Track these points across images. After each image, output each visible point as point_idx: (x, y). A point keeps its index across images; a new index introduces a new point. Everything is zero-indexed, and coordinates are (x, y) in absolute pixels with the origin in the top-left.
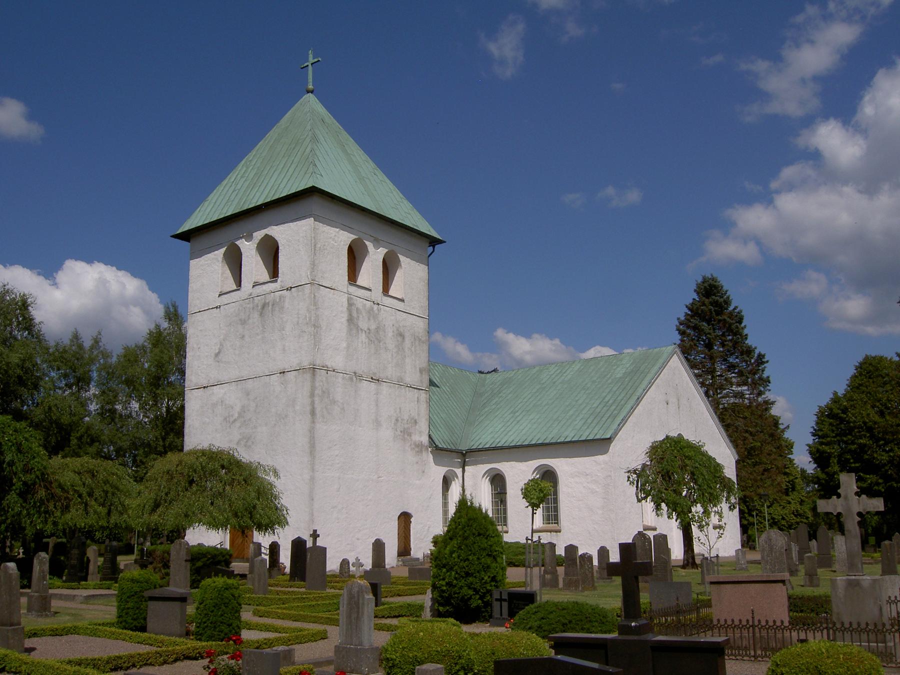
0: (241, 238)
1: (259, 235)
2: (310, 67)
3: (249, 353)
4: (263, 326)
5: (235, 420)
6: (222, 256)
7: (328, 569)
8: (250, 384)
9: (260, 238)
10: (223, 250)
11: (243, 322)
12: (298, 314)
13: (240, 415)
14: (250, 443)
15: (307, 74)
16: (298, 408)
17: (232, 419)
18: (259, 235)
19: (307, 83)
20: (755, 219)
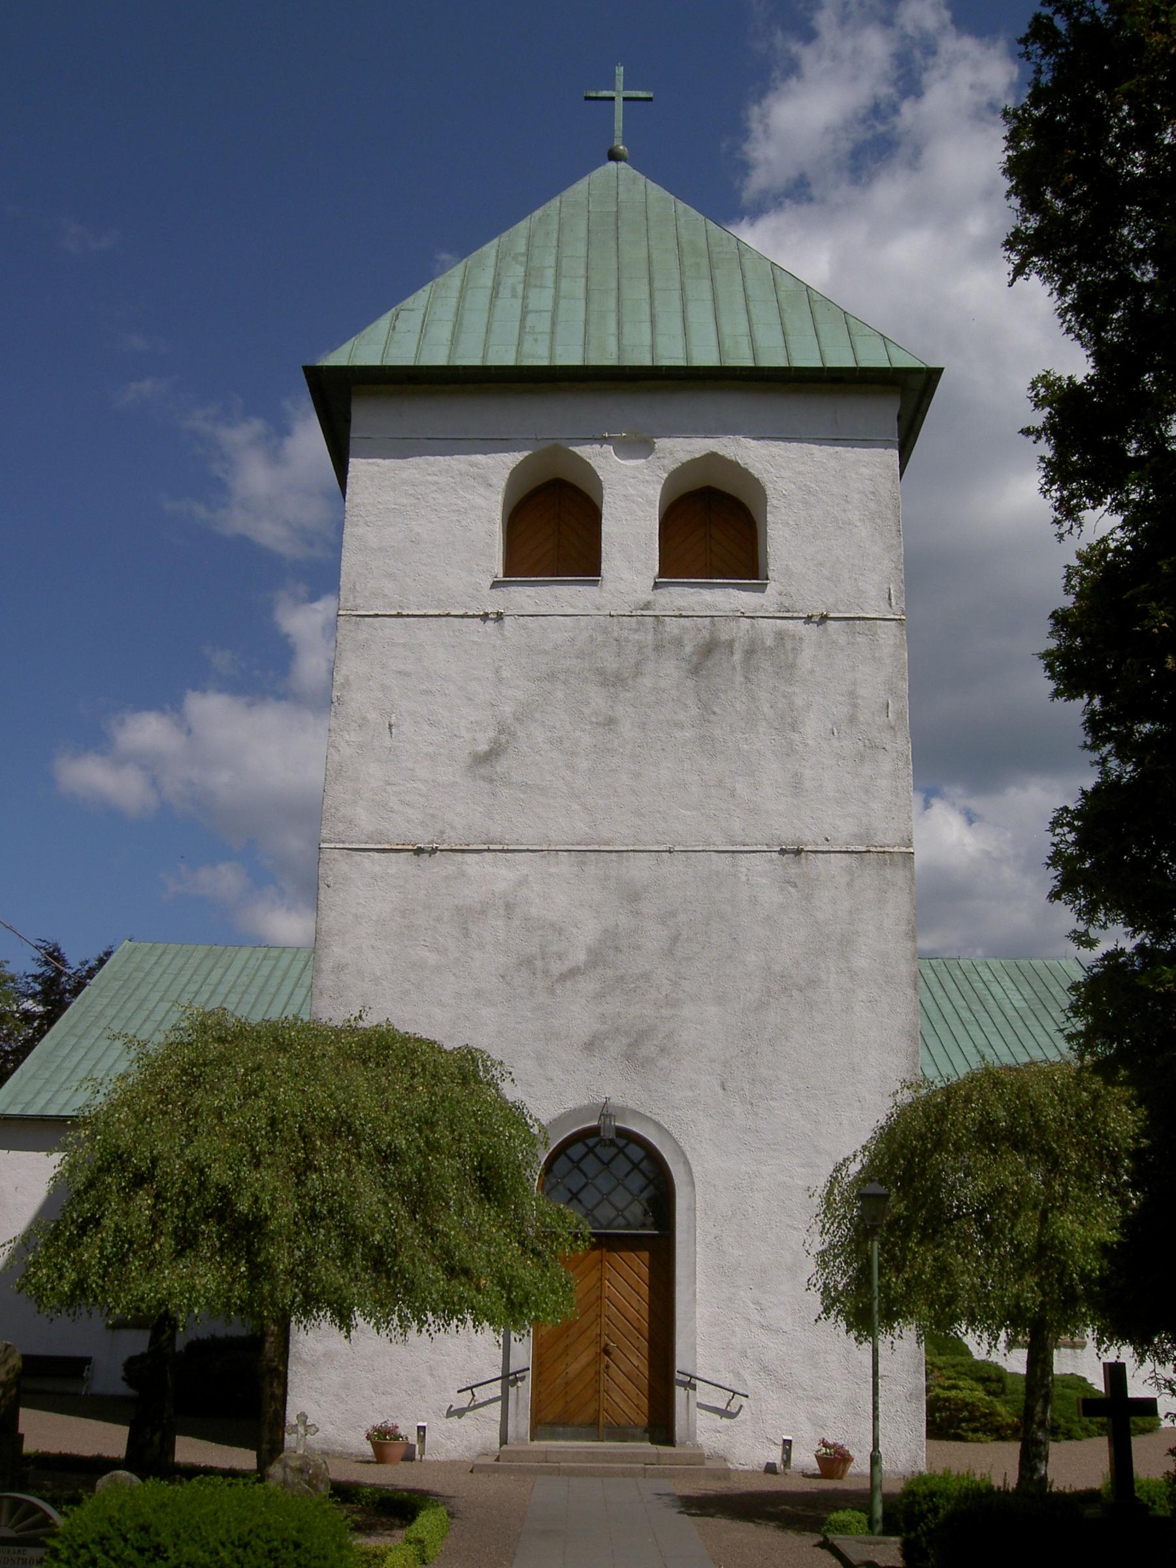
0: (603, 441)
1: (680, 450)
2: (619, 104)
3: (637, 776)
4: (705, 707)
5: (573, 973)
6: (506, 474)
7: (125, 1430)
8: (640, 869)
9: (685, 457)
10: (519, 457)
11: (613, 681)
12: (852, 694)
13: (596, 958)
14: (648, 1049)
15: (612, 111)
16: (861, 963)
17: (557, 968)
18: (680, 450)
19: (612, 138)
20: (147, 731)
